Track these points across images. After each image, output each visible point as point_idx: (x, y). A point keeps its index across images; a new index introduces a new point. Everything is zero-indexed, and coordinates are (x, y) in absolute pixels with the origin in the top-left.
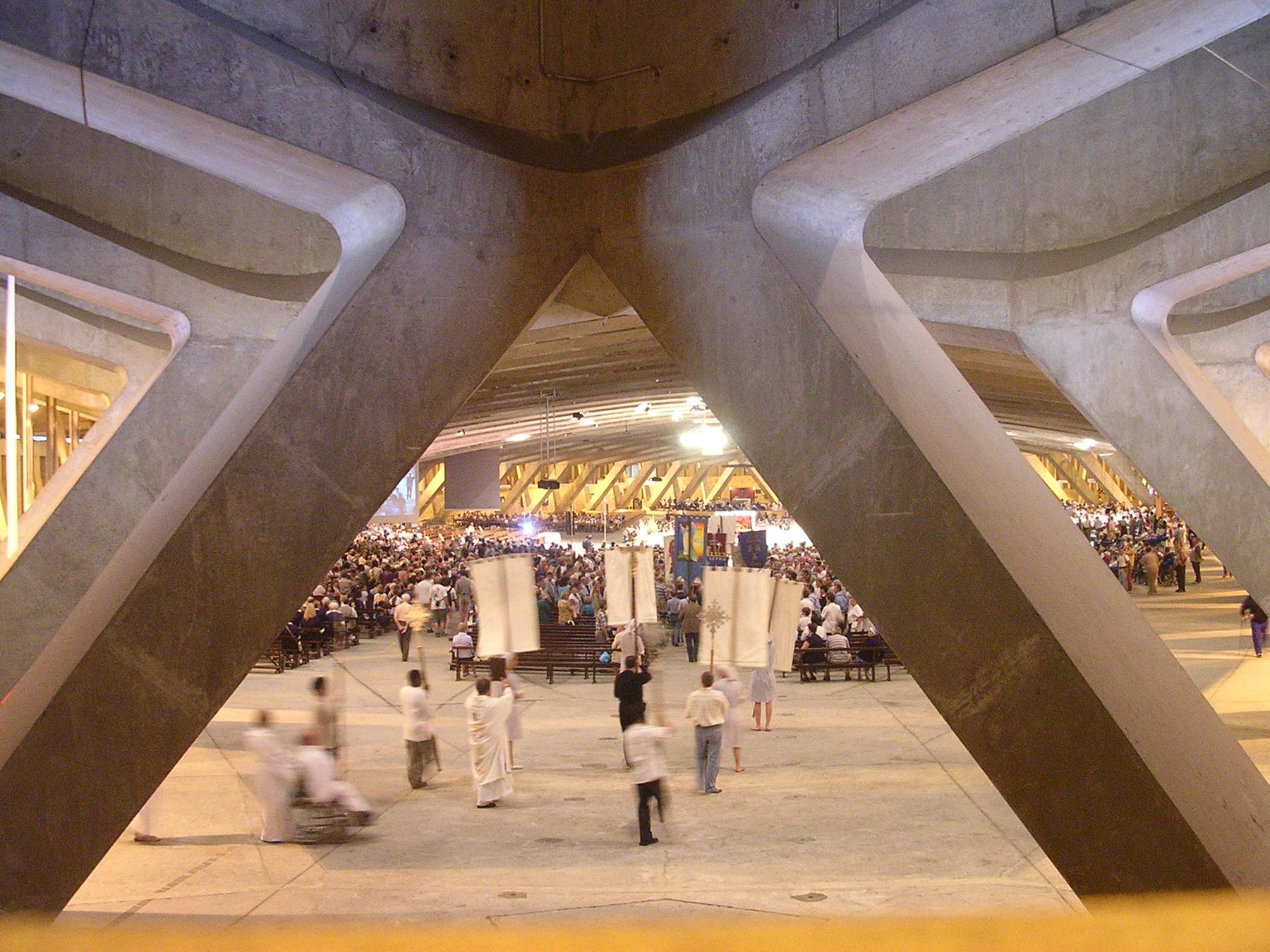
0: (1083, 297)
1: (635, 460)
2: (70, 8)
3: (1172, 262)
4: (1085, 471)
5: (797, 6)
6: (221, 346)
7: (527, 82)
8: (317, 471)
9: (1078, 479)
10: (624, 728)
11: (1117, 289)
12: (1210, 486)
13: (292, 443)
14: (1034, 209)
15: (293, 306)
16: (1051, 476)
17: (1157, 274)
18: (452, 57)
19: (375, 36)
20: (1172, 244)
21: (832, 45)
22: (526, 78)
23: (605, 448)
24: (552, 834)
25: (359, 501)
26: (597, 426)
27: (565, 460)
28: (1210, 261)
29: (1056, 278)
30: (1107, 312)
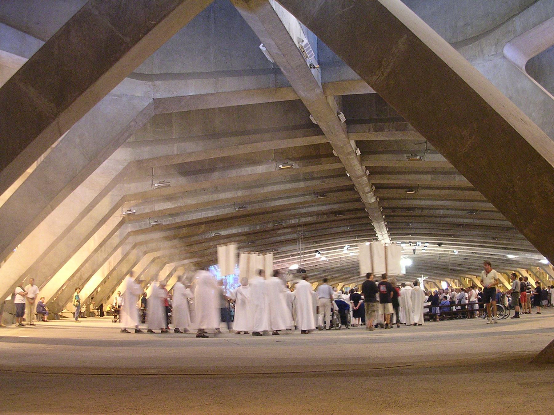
0: (482, 51)
1: (348, 282)
3: (519, 29)
4: (548, 276)
6: (116, 98)
8: (110, 25)
9: (544, 279)
11: (496, 44)
12: (545, 120)
13: (100, 13)
14: (460, 24)
15: (148, 83)
16: (533, 281)
20: (518, 23)
23: (334, 276)
25: (127, 39)
26: (328, 260)
27: (316, 282)
29: (471, 45)
30: (492, 55)
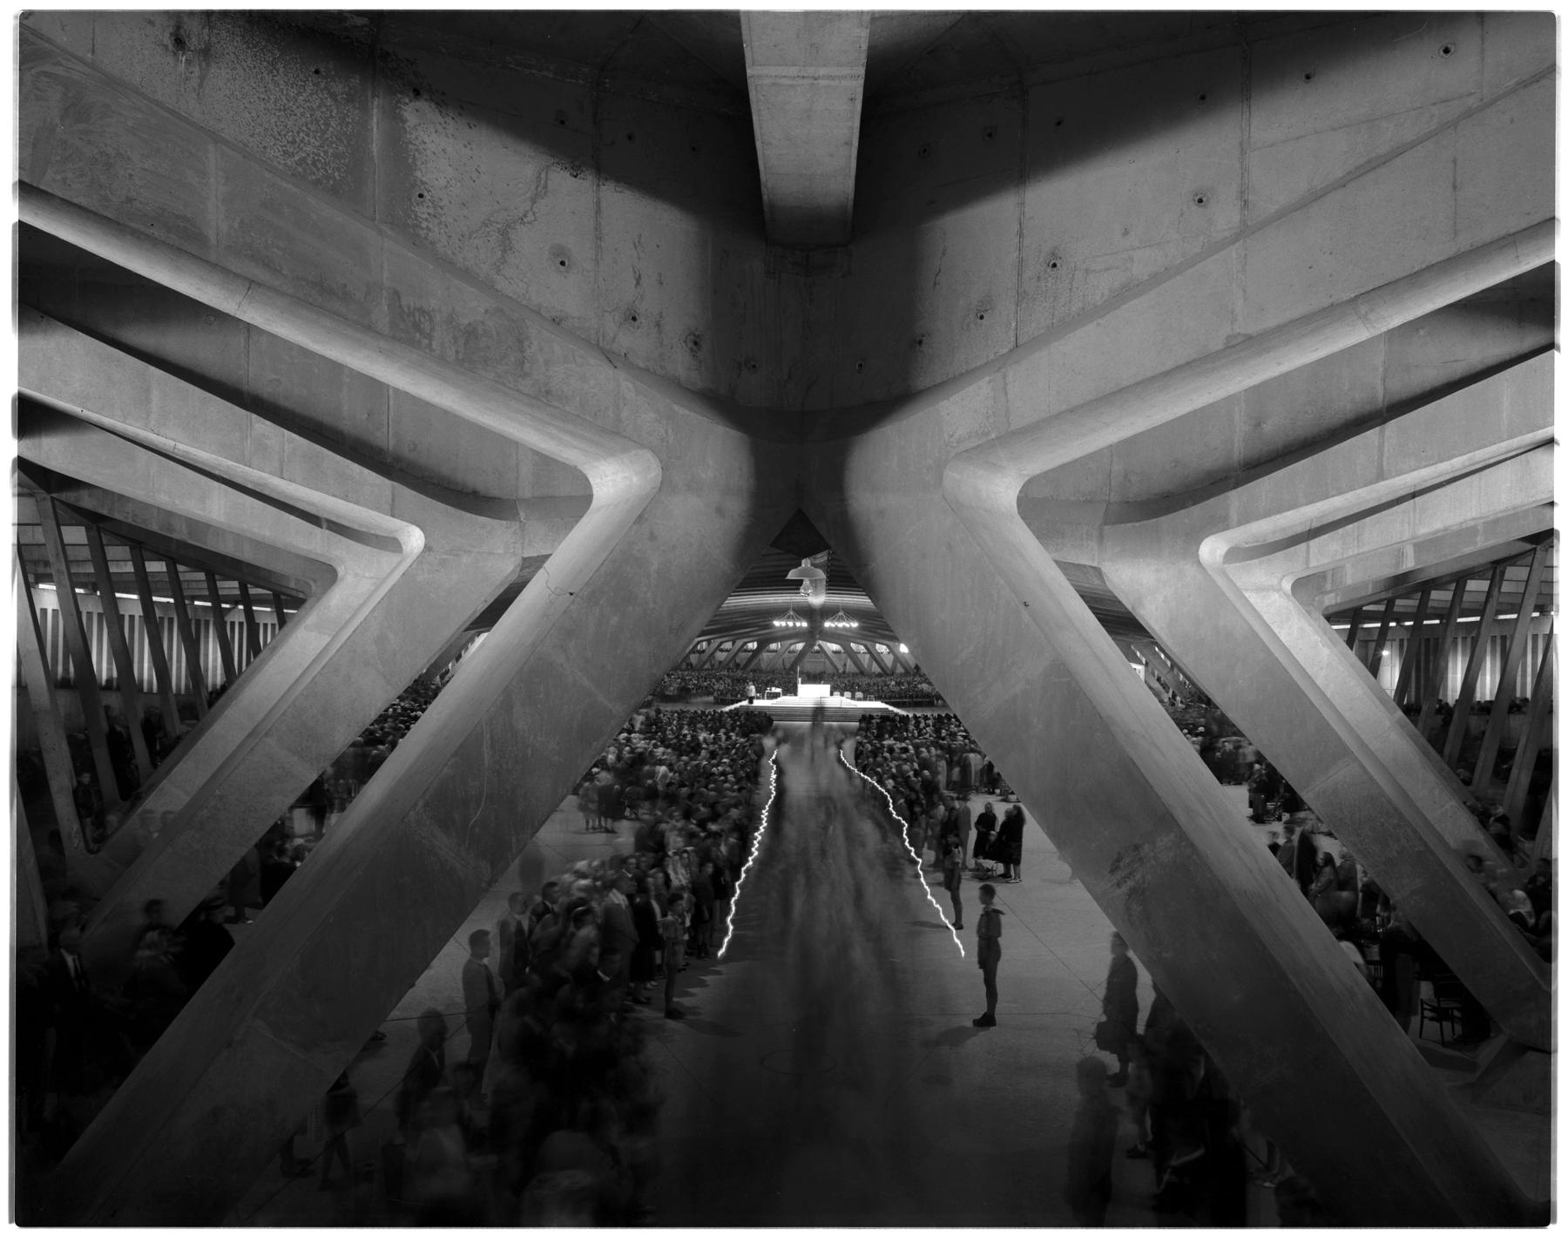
2: (1348, 390)
5: (982, 317)
7: (754, 366)
10: (707, 986)
17: (1219, 524)
18: (696, 343)
19: (636, 324)
21: (1011, 351)
22: (753, 363)
24: (1093, 1023)
28: (1267, 514)
